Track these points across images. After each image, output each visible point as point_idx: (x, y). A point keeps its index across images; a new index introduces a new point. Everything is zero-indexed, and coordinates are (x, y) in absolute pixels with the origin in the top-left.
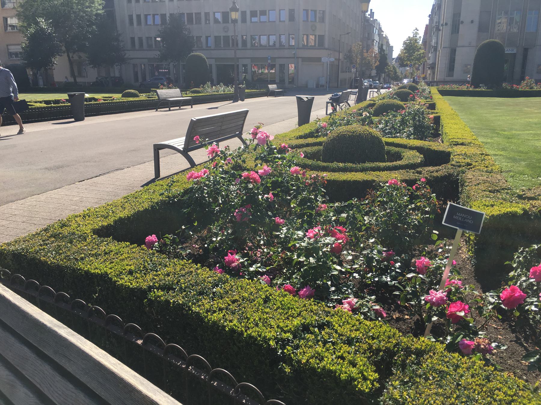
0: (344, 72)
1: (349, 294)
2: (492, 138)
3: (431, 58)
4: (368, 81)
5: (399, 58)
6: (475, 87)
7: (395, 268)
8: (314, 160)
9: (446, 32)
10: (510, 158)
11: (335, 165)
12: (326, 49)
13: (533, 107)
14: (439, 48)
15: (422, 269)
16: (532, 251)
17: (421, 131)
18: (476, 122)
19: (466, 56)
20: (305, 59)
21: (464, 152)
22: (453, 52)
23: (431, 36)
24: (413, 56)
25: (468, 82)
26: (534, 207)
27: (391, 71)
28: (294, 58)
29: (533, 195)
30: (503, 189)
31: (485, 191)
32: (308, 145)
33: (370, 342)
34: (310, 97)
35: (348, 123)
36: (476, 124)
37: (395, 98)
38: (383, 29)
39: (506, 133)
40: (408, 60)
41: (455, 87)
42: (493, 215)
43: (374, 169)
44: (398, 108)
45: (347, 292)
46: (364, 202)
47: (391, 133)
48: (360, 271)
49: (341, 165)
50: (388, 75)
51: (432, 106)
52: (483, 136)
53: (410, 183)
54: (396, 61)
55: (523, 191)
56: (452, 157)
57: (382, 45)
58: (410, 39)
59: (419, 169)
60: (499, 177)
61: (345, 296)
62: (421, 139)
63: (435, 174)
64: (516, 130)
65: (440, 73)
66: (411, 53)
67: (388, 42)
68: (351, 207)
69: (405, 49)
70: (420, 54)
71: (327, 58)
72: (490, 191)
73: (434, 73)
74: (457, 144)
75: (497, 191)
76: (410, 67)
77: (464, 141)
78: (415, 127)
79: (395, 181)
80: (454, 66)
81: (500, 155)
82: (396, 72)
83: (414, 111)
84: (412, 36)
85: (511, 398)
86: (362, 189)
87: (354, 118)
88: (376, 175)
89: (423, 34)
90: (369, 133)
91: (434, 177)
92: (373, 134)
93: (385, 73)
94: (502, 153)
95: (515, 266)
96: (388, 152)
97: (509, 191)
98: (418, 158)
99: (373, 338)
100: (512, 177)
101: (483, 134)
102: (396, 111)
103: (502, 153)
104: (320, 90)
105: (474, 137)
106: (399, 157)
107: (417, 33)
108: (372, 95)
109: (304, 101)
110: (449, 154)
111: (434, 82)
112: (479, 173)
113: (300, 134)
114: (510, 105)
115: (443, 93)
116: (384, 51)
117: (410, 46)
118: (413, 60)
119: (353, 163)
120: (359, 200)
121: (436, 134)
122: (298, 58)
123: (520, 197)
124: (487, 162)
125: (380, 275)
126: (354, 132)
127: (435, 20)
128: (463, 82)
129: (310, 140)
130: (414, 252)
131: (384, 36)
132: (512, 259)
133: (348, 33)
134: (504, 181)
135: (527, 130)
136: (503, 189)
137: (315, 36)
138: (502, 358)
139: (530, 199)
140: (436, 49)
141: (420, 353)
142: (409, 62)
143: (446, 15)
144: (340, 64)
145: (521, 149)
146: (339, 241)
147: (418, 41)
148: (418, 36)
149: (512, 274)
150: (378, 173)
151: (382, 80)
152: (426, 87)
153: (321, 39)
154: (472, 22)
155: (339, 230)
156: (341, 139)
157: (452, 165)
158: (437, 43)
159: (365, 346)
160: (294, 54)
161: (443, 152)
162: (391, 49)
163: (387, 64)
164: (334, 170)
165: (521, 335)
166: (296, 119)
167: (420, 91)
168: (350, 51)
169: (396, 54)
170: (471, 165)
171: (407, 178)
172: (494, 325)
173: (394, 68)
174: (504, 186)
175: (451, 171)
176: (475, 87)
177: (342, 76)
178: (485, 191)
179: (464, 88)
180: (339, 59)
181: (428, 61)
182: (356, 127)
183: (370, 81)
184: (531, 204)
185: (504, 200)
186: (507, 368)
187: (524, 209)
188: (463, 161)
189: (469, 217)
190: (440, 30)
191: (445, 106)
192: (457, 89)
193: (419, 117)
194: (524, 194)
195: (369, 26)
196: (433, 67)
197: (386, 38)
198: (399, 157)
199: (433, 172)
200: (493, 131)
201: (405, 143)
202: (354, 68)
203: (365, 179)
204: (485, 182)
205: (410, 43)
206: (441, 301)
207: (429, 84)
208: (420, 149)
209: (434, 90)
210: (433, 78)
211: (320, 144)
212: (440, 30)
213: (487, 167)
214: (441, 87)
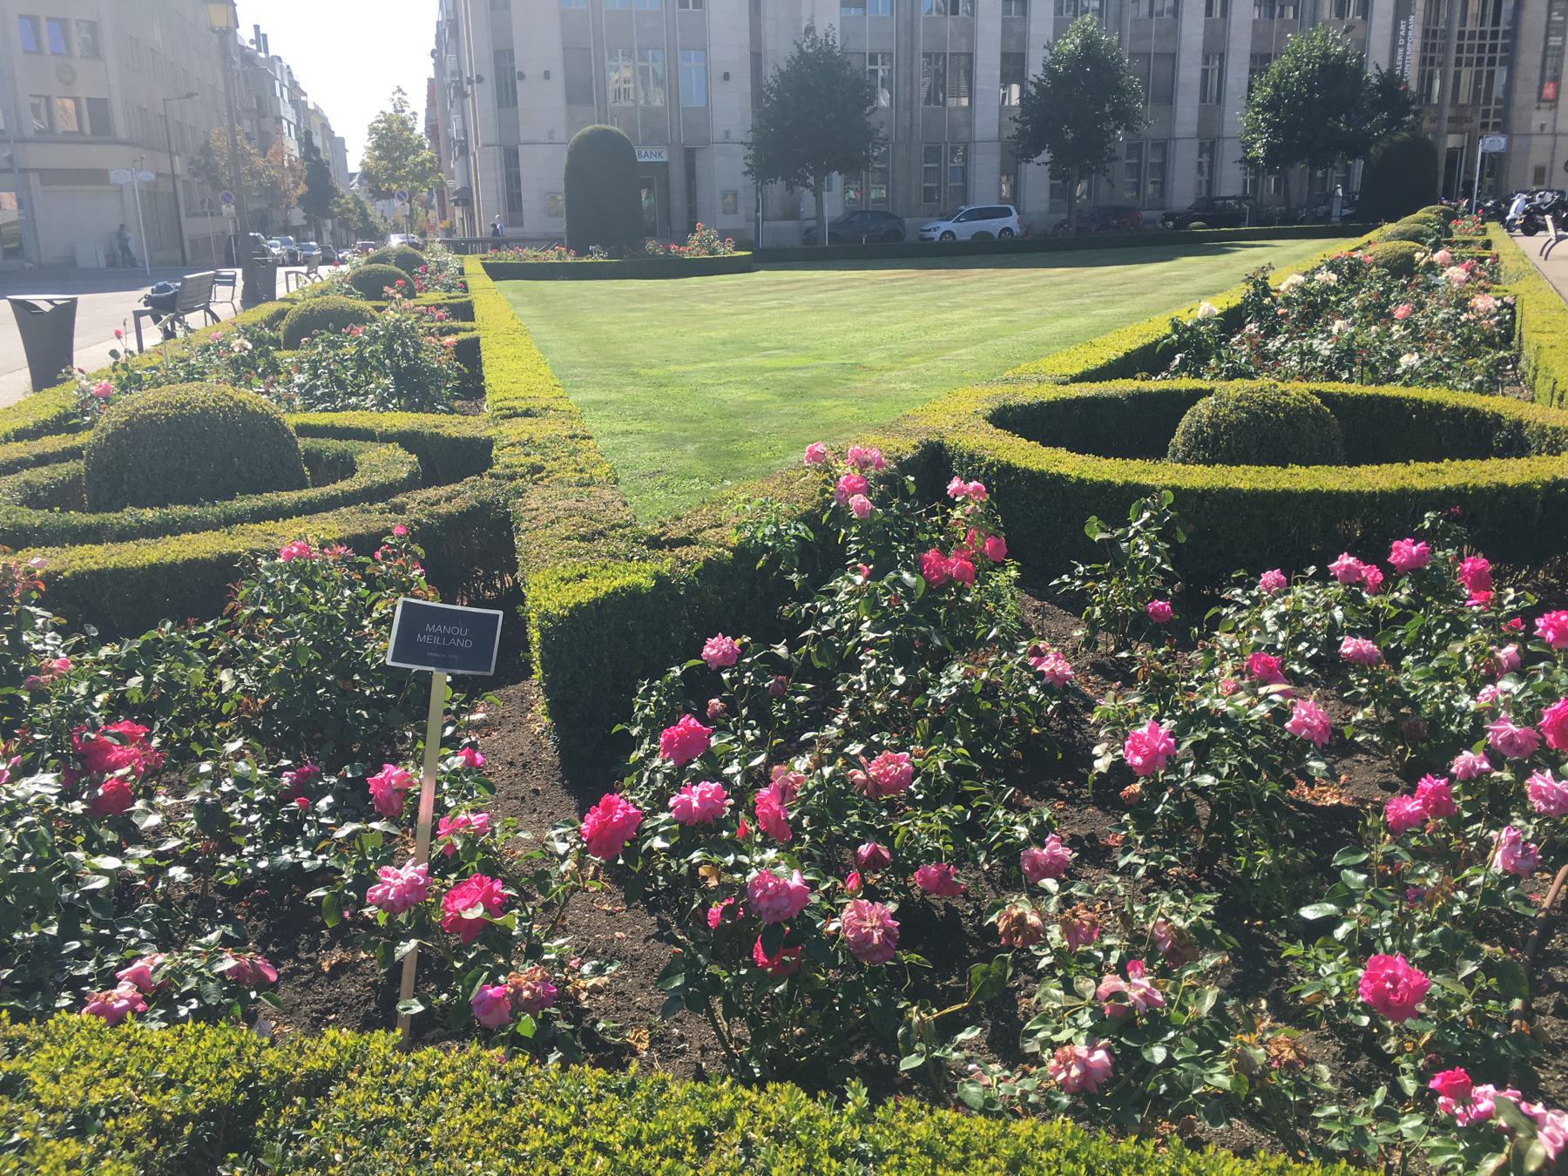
0: (196, 215)
1: (142, 943)
2: (619, 387)
3: (457, 175)
4: (283, 243)
5: (367, 175)
6: (579, 255)
7: (318, 815)
8: (51, 511)
9: (482, 99)
10: (661, 438)
11: (127, 516)
12: (121, 143)
13: (720, 299)
14: (472, 147)
15: (389, 800)
16: (670, 686)
17: (415, 387)
18: (584, 348)
19: (545, 172)
20: (51, 176)
21: (526, 437)
22: (511, 159)
23: (446, 113)
24: (404, 166)
25: (560, 242)
26: (684, 564)
27: (350, 211)
28: (10, 171)
29: (684, 534)
30: (613, 528)
31: (568, 538)
32: (42, 460)
33: (153, 1101)
34: (60, 298)
35: (194, 374)
36: (584, 354)
37: (348, 292)
38: (302, 87)
39: (654, 372)
40: (392, 178)
41: (530, 255)
42: (578, 605)
43: (259, 516)
44: (358, 318)
45: (133, 942)
46: (201, 630)
47: (331, 397)
48: (193, 853)
49: (149, 514)
50: (344, 223)
51: (465, 311)
52: (598, 384)
53: (366, 544)
54: (360, 182)
55: (663, 525)
56: (495, 452)
57: (308, 134)
58: (388, 120)
59: (399, 499)
60: (607, 494)
61: (128, 954)
62: (418, 408)
63: (444, 508)
64: (678, 363)
65: (489, 213)
66: (399, 158)
67: (325, 126)
68: (151, 652)
69: (378, 146)
70: (422, 163)
71: (130, 172)
72: (583, 538)
73: (472, 217)
74: (514, 414)
75: (601, 534)
76: (400, 198)
77: (531, 404)
78: (400, 377)
79: (300, 548)
80: (520, 195)
81: (639, 432)
82: (364, 215)
83: (386, 329)
84: (390, 110)
85: (561, 1137)
86: (204, 590)
87: (219, 357)
88: (264, 532)
89: (425, 106)
90: (236, 405)
91: (439, 516)
92: (249, 408)
93: (332, 216)
94: (642, 426)
95: (635, 732)
96: (313, 458)
97: (627, 531)
98: (402, 463)
99: (168, 1084)
100: (664, 486)
101: (599, 378)
102: (337, 331)
103: (642, 426)
104: (117, 271)
105: (559, 391)
106: (345, 466)
107: (403, 102)
108: (287, 283)
109: (43, 313)
110: (489, 444)
111: (477, 241)
112: (560, 489)
113: (19, 424)
114: (666, 299)
115: (497, 272)
116: (316, 151)
117: (391, 139)
118: (404, 178)
119: (193, 502)
120: (181, 624)
121: (472, 388)
122: (23, 171)
123: (655, 543)
124: (581, 459)
125: (272, 850)
126: (183, 406)
127: (451, 64)
128: (547, 241)
129: (51, 444)
130: (400, 747)
131: (311, 106)
132: (628, 717)
133: (190, 96)
134: (619, 505)
135: (702, 361)
136: (613, 528)
137: (77, 100)
138: (622, 993)
139: (675, 543)
140: (464, 150)
141: (317, 1085)
142: (394, 187)
143: (475, 56)
144: (181, 193)
145: (689, 412)
146: (119, 773)
147: (410, 124)
148: (408, 112)
149: (636, 755)
150: (269, 526)
151: (326, 237)
152: (450, 257)
153: (99, 110)
154: (547, 75)
155: (116, 736)
156: (138, 431)
157: (492, 476)
158: (465, 132)
159: (134, 1123)
160: (10, 159)
161: (472, 442)
162: (339, 146)
163: (333, 191)
164: (124, 535)
165: (670, 912)
166: (25, 376)
167: (432, 267)
168: (206, 150)
169: (354, 164)
170: (541, 469)
171: (361, 531)
172: (606, 907)
173: (358, 202)
174: (617, 518)
175: (489, 494)
176: (579, 255)
177: (192, 227)
178: (568, 538)
179: (551, 257)
180: (174, 177)
181: (450, 183)
182: (212, 390)
183: (290, 243)
184: (678, 558)
185: (614, 556)
186: (633, 1019)
187: (658, 577)
188: (523, 459)
189: (460, 631)
190: (466, 95)
191: (499, 309)
192: (533, 261)
193: (404, 345)
194: (664, 534)
195: (253, 78)
196: (465, 198)
197: (317, 112)
198: (345, 466)
199: (438, 502)
200: (625, 368)
201: (368, 425)
202: (226, 201)
203: (225, 551)
204: (570, 513)
205: (389, 129)
206: (410, 892)
207: (460, 248)
208: (408, 440)
209: (473, 265)
210: (473, 231)
211: (73, 454)
212: (466, 95)
213: (581, 471)
214: (492, 256)
